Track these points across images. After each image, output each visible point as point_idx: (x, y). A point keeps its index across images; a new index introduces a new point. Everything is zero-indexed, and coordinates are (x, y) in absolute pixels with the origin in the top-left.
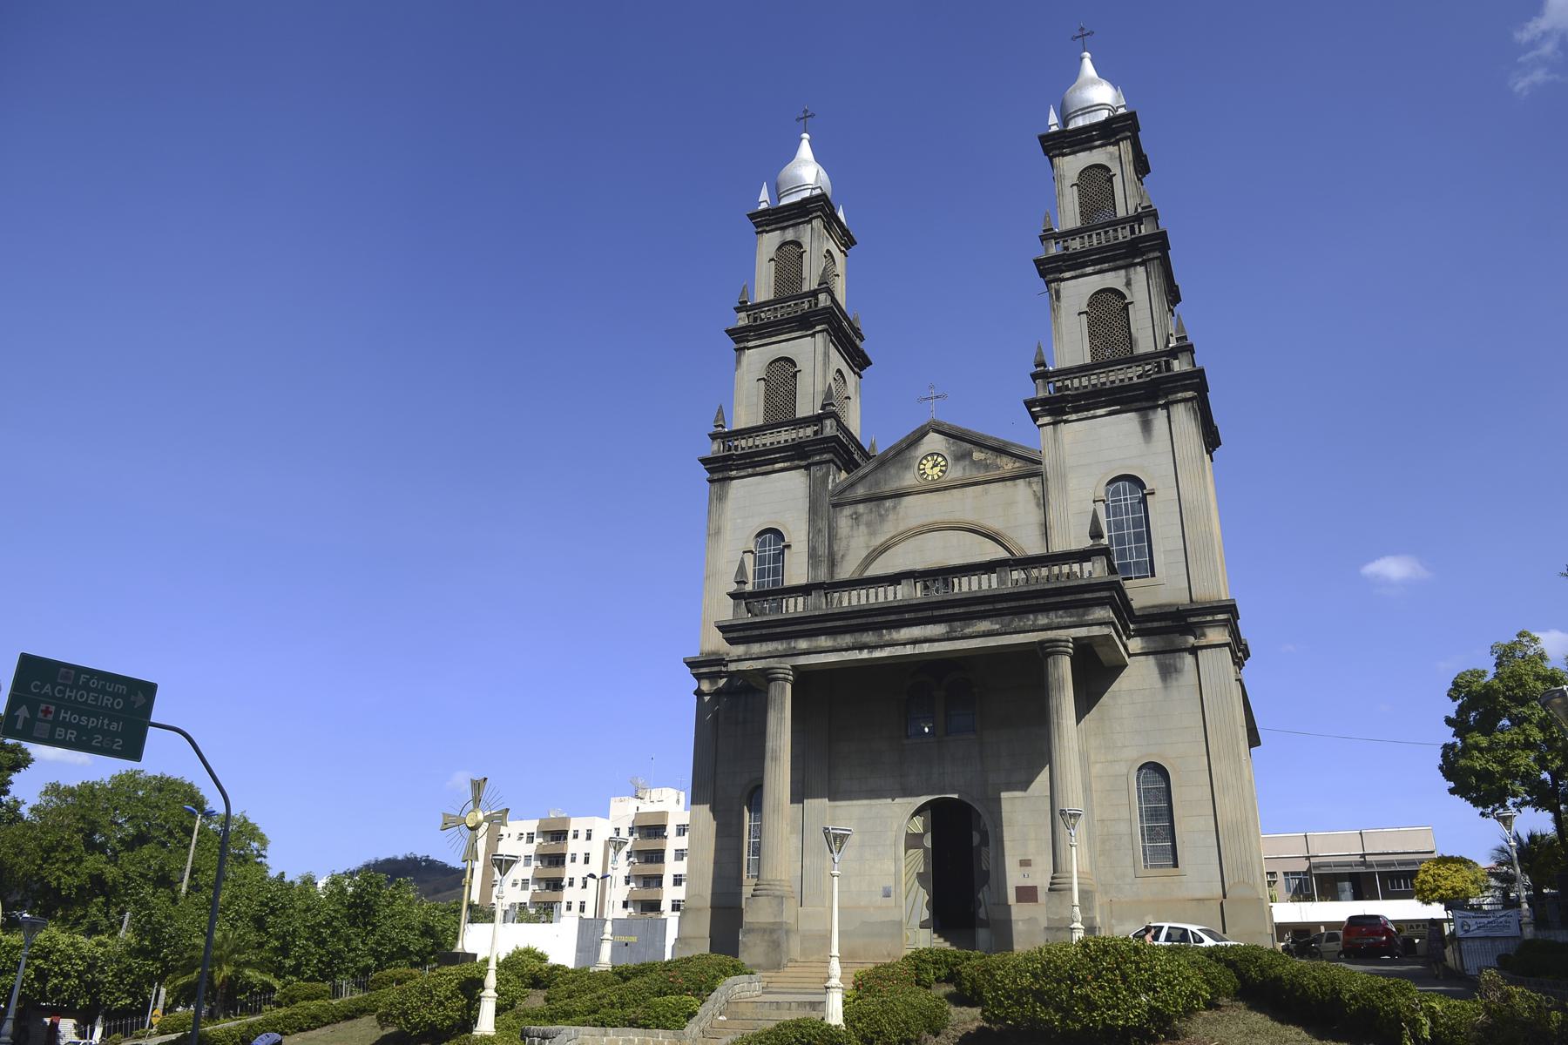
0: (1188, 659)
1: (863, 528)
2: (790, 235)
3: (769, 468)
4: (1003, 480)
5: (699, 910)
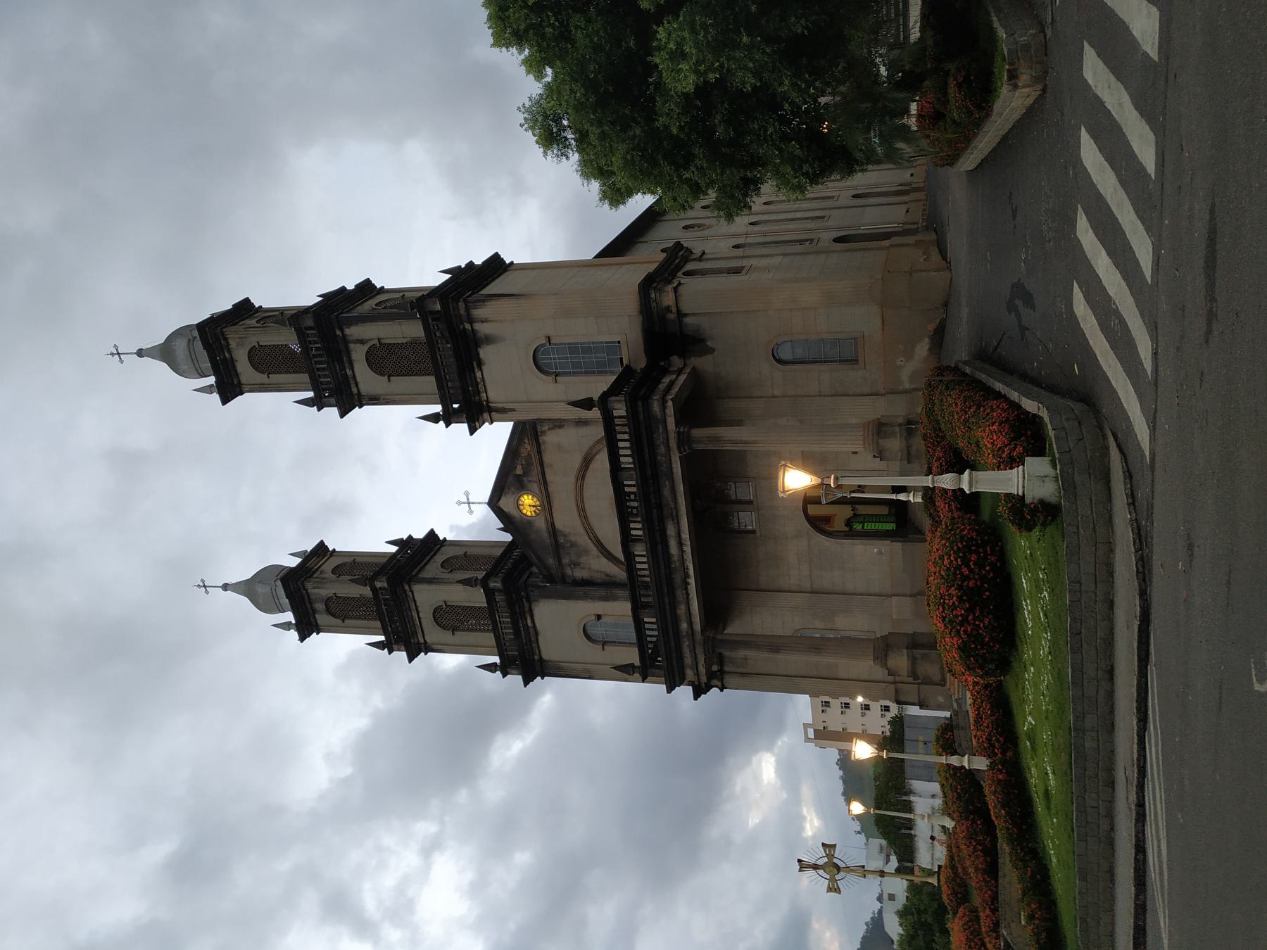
0: (688, 320)
1: (581, 560)
2: (320, 606)
3: (532, 631)
4: (540, 453)
5: (896, 690)
